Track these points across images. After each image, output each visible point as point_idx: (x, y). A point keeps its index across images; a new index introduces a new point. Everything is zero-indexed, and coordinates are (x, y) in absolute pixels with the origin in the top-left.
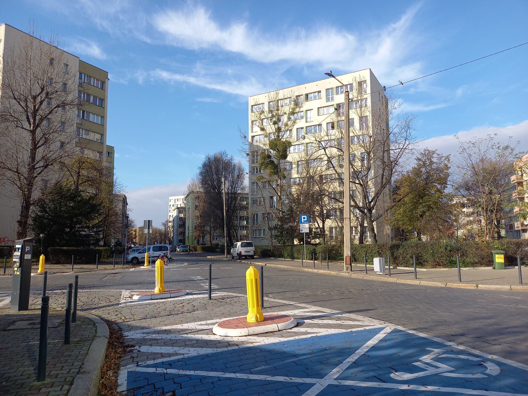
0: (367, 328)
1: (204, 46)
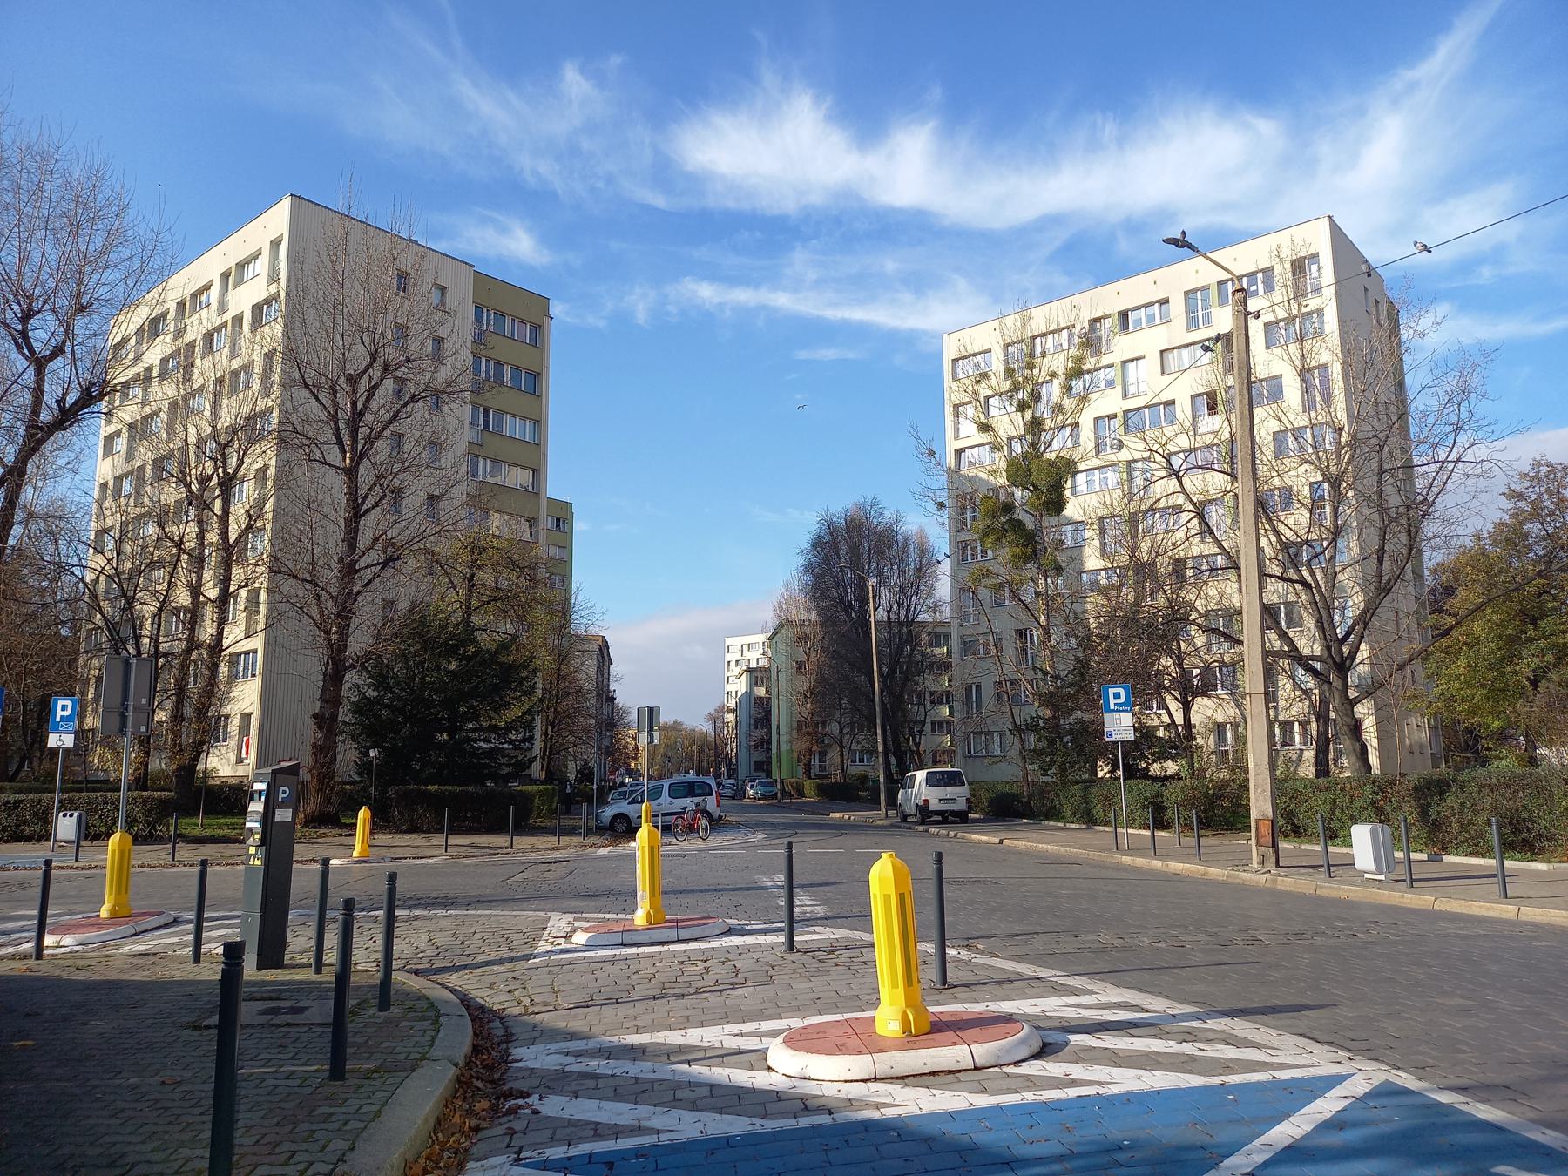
0: (1283, 1075)
1: (816, 199)
